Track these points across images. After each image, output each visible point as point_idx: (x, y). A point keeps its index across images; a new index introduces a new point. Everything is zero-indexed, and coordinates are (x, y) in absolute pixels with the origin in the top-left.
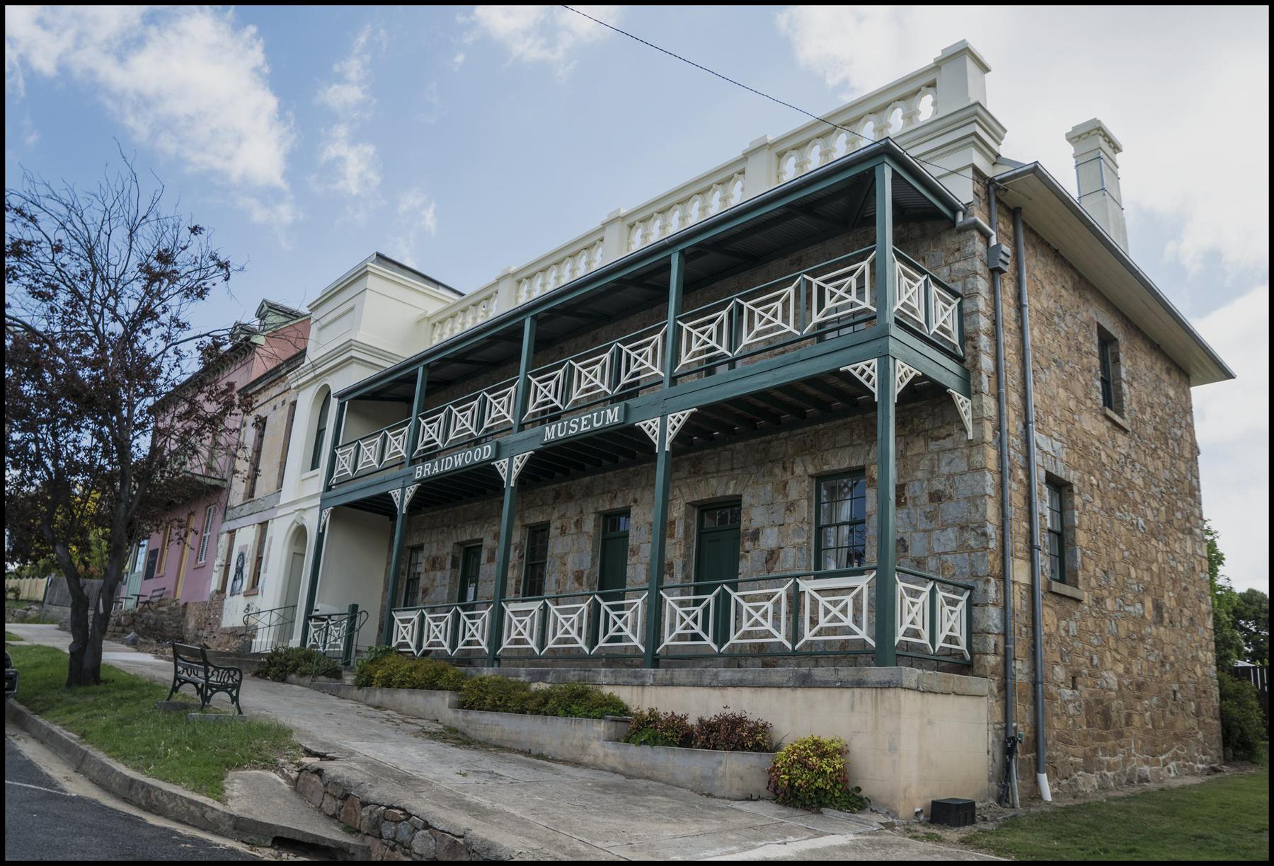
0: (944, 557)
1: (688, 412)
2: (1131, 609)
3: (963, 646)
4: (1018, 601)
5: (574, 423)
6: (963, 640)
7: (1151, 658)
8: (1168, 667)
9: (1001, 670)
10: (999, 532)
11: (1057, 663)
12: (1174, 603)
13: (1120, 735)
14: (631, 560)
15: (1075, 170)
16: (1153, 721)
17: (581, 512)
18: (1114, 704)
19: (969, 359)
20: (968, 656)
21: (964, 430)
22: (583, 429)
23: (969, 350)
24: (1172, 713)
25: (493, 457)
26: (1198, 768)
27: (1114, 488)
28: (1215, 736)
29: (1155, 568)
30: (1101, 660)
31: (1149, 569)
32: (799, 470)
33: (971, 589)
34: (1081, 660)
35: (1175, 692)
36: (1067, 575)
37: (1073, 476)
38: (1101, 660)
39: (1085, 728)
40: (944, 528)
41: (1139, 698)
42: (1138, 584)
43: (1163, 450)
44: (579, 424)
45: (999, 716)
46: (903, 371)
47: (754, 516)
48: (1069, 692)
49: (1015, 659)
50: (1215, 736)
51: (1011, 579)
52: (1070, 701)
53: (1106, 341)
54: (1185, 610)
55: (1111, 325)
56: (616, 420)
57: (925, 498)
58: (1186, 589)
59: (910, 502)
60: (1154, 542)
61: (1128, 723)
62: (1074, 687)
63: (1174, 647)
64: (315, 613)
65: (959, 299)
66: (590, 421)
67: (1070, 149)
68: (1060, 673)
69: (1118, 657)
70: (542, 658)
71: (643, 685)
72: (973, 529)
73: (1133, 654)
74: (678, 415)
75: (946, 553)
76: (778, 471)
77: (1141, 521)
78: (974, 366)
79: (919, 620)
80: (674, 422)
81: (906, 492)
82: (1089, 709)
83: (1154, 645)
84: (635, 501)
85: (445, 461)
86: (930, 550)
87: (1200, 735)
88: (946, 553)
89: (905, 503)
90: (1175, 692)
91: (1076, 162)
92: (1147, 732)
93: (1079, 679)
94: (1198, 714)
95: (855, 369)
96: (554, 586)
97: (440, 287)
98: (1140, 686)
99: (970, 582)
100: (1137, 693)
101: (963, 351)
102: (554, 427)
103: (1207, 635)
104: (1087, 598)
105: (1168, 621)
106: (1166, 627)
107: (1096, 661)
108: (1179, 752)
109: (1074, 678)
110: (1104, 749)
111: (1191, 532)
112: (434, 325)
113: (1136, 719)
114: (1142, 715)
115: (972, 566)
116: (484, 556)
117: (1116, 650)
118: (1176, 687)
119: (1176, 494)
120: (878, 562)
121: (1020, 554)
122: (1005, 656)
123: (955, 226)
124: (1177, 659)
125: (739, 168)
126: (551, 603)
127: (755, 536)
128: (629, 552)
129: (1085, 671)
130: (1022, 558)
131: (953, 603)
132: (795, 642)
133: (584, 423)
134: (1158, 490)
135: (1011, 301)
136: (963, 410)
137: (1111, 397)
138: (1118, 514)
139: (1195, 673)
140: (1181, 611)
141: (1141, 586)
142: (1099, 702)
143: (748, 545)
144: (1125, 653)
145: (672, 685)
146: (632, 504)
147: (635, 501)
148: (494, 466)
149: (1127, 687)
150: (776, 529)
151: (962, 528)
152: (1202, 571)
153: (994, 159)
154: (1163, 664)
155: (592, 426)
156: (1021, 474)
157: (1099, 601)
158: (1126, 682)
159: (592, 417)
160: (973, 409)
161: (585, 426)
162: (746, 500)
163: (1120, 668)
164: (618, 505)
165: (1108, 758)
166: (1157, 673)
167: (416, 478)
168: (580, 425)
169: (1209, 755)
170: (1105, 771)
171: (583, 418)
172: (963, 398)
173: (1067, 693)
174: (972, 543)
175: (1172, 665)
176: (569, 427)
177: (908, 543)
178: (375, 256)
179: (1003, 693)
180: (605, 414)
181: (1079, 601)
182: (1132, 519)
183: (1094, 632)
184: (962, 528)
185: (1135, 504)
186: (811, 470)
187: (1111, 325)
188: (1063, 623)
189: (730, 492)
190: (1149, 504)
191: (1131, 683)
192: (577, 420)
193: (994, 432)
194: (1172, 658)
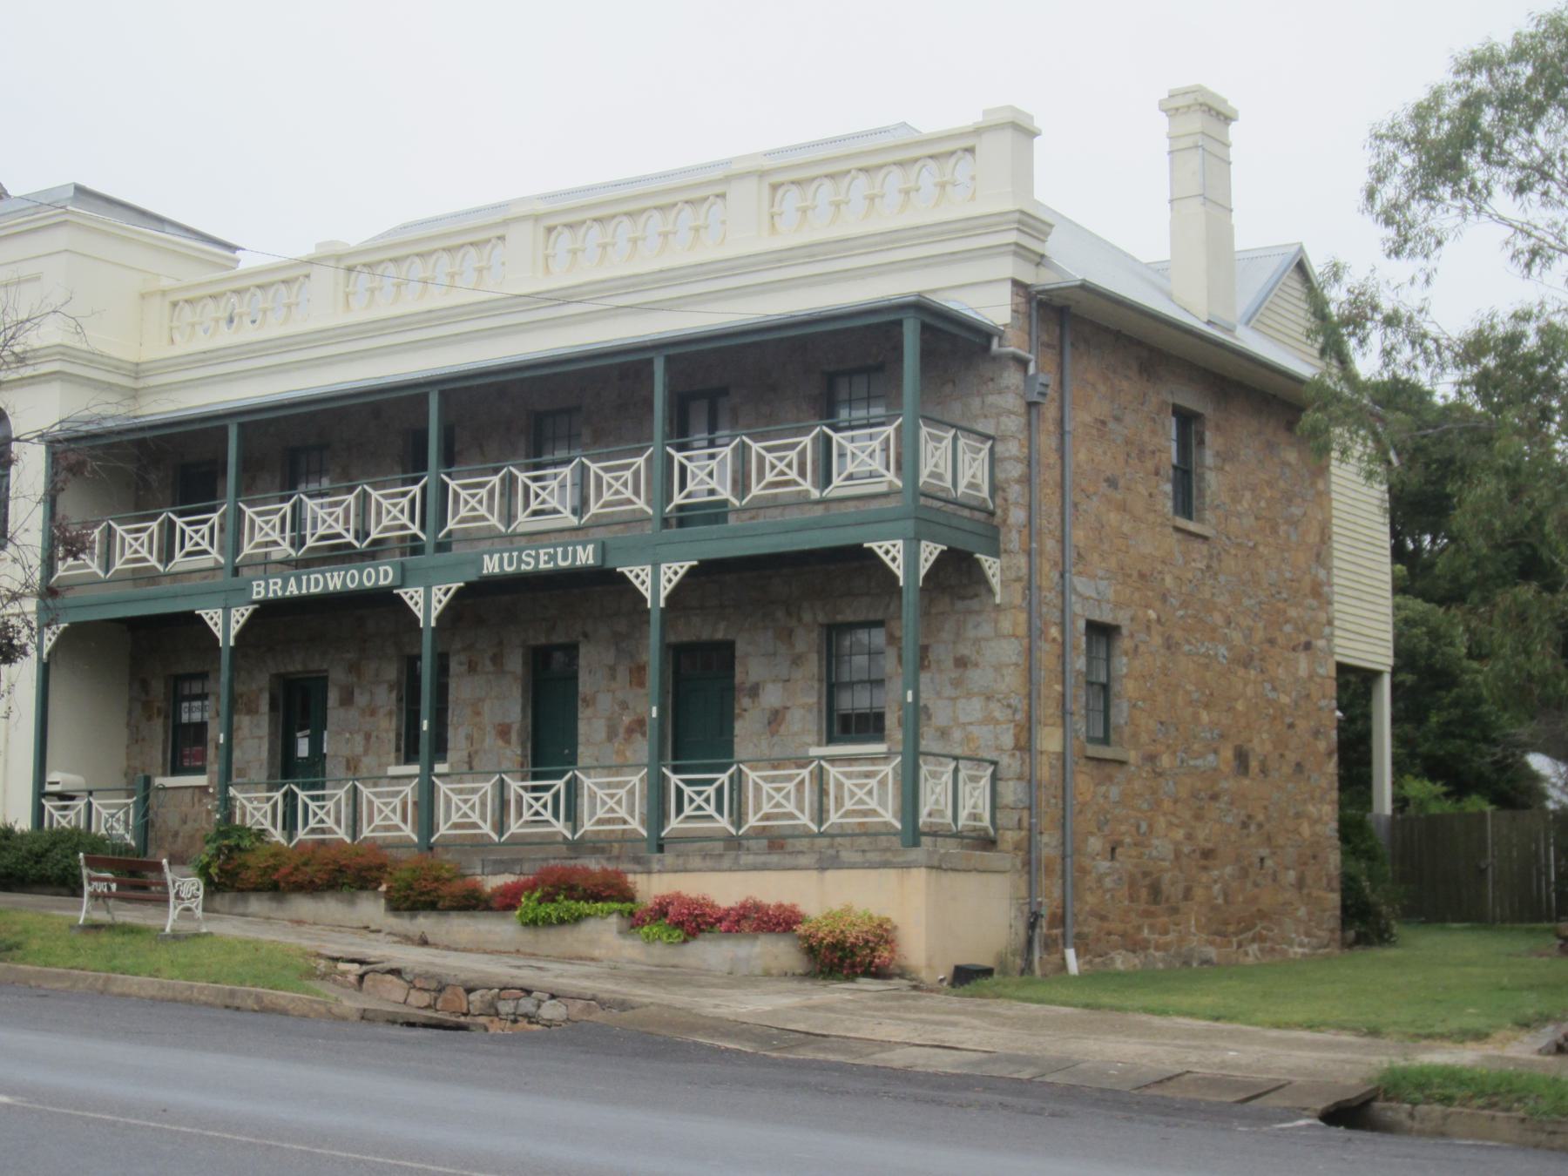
0: (970, 728)
1: (687, 565)
2: (1199, 762)
3: (986, 822)
4: (1045, 772)
5: (529, 555)
6: (987, 816)
7: (1229, 819)
8: (1253, 828)
9: (1025, 845)
10: (1026, 701)
11: (1092, 834)
12: (1268, 747)
13: (1174, 910)
14: (584, 713)
15: (1167, 158)
16: (1226, 895)
17: (500, 643)
18: (1167, 877)
19: (999, 512)
20: (992, 832)
21: (990, 591)
22: (542, 566)
23: (999, 501)
24: (1256, 885)
25: (398, 583)
26: (1296, 953)
27: (1182, 617)
28: (1328, 914)
29: (1240, 706)
30: (1150, 826)
31: (1231, 709)
32: (807, 617)
33: (994, 763)
34: (1123, 828)
35: (1262, 860)
36: (1112, 732)
37: (1122, 618)
38: (1150, 826)
39: (1126, 903)
40: (969, 695)
41: (1205, 868)
42: (1211, 731)
43: (1267, 545)
44: (537, 558)
45: (1024, 892)
46: (928, 550)
47: (750, 668)
48: (1107, 864)
49: (1041, 833)
50: (1328, 914)
51: (1038, 747)
52: (1108, 874)
53: (1187, 420)
54: (1287, 753)
55: (1190, 400)
56: (591, 561)
57: (950, 663)
58: (1291, 726)
59: (933, 666)
60: (1241, 672)
61: (1188, 894)
62: (1113, 858)
63: (1266, 803)
64: (49, 788)
65: (989, 443)
66: (553, 557)
67: (1163, 121)
68: (1095, 844)
69: (1176, 821)
70: (504, 844)
71: (649, 872)
72: (999, 701)
73: (1198, 817)
74: (675, 566)
75: (971, 724)
76: (780, 614)
77: (1223, 650)
78: (1005, 521)
79: (942, 800)
80: (670, 574)
81: (930, 655)
82: (1133, 883)
83: (1232, 803)
84: (586, 635)
85: (308, 580)
86: (955, 719)
87: (1302, 912)
88: (971, 724)
89: (929, 666)
90: (1262, 860)
91: (1171, 145)
92: (1215, 908)
93: (1119, 850)
94: (1300, 884)
95: (880, 547)
96: (463, 743)
97: (168, 229)
98: (1207, 854)
99: (993, 756)
100: (1203, 862)
101: (994, 503)
102: (496, 557)
103: (1324, 783)
104: (1132, 756)
105: (1257, 770)
106: (1253, 779)
107: (1144, 827)
108: (1264, 932)
109: (1113, 850)
110: (1152, 928)
111: (1308, 646)
112: (175, 304)
113: (1199, 893)
114: (1208, 888)
115: (997, 738)
116: (333, 697)
117: (1173, 814)
118: (1264, 852)
119: (1285, 600)
120: (897, 538)
121: (1051, 721)
122: (1030, 830)
123: (951, 550)
124: (1268, 819)
125: (718, 190)
126: (512, 779)
127: (754, 691)
128: (580, 703)
129: (1128, 840)
130: (1052, 725)
131: (974, 779)
132: (821, 822)
133: (543, 558)
134: (1253, 602)
135: (1052, 428)
136: (990, 573)
137: (1186, 501)
138: (1186, 648)
139: (1299, 834)
140: (1282, 756)
141: (1216, 732)
142: (1146, 874)
143: (745, 702)
144: (1187, 815)
145: (686, 870)
146: (581, 638)
147: (586, 635)
148: (398, 596)
149: (1188, 856)
150: (780, 685)
151: (988, 698)
152: (1324, 697)
153: (1037, 259)
154: (1245, 825)
155: (556, 563)
156: (1054, 632)
157: (1152, 758)
158: (1186, 849)
159: (556, 553)
160: (1002, 570)
161: (546, 562)
162: (741, 648)
163: (1179, 834)
164: (558, 638)
165: (1156, 936)
166: (1233, 837)
167: (255, 597)
168: (539, 560)
169: (1316, 936)
170: (1152, 951)
171: (542, 552)
172: (991, 560)
173: (1104, 865)
174: (997, 714)
175: (1260, 826)
176: (520, 561)
177: (931, 711)
178: (71, 193)
179: (1026, 868)
180: (575, 552)
181: (1122, 763)
182: (1208, 649)
183: (1141, 795)
184: (988, 698)
185: (1214, 629)
186: (821, 618)
187: (1190, 400)
188: (1103, 789)
189: (719, 636)
190: (1237, 624)
191: (1194, 851)
192: (533, 553)
193: (1024, 592)
194: (1261, 817)
